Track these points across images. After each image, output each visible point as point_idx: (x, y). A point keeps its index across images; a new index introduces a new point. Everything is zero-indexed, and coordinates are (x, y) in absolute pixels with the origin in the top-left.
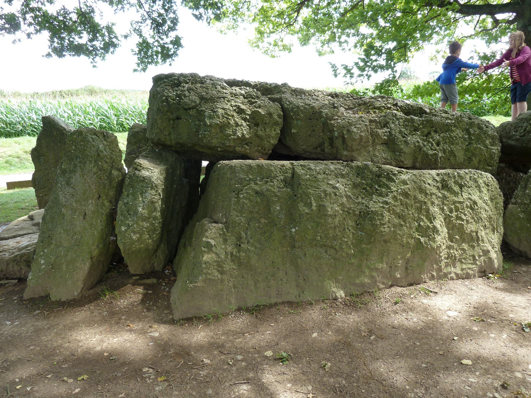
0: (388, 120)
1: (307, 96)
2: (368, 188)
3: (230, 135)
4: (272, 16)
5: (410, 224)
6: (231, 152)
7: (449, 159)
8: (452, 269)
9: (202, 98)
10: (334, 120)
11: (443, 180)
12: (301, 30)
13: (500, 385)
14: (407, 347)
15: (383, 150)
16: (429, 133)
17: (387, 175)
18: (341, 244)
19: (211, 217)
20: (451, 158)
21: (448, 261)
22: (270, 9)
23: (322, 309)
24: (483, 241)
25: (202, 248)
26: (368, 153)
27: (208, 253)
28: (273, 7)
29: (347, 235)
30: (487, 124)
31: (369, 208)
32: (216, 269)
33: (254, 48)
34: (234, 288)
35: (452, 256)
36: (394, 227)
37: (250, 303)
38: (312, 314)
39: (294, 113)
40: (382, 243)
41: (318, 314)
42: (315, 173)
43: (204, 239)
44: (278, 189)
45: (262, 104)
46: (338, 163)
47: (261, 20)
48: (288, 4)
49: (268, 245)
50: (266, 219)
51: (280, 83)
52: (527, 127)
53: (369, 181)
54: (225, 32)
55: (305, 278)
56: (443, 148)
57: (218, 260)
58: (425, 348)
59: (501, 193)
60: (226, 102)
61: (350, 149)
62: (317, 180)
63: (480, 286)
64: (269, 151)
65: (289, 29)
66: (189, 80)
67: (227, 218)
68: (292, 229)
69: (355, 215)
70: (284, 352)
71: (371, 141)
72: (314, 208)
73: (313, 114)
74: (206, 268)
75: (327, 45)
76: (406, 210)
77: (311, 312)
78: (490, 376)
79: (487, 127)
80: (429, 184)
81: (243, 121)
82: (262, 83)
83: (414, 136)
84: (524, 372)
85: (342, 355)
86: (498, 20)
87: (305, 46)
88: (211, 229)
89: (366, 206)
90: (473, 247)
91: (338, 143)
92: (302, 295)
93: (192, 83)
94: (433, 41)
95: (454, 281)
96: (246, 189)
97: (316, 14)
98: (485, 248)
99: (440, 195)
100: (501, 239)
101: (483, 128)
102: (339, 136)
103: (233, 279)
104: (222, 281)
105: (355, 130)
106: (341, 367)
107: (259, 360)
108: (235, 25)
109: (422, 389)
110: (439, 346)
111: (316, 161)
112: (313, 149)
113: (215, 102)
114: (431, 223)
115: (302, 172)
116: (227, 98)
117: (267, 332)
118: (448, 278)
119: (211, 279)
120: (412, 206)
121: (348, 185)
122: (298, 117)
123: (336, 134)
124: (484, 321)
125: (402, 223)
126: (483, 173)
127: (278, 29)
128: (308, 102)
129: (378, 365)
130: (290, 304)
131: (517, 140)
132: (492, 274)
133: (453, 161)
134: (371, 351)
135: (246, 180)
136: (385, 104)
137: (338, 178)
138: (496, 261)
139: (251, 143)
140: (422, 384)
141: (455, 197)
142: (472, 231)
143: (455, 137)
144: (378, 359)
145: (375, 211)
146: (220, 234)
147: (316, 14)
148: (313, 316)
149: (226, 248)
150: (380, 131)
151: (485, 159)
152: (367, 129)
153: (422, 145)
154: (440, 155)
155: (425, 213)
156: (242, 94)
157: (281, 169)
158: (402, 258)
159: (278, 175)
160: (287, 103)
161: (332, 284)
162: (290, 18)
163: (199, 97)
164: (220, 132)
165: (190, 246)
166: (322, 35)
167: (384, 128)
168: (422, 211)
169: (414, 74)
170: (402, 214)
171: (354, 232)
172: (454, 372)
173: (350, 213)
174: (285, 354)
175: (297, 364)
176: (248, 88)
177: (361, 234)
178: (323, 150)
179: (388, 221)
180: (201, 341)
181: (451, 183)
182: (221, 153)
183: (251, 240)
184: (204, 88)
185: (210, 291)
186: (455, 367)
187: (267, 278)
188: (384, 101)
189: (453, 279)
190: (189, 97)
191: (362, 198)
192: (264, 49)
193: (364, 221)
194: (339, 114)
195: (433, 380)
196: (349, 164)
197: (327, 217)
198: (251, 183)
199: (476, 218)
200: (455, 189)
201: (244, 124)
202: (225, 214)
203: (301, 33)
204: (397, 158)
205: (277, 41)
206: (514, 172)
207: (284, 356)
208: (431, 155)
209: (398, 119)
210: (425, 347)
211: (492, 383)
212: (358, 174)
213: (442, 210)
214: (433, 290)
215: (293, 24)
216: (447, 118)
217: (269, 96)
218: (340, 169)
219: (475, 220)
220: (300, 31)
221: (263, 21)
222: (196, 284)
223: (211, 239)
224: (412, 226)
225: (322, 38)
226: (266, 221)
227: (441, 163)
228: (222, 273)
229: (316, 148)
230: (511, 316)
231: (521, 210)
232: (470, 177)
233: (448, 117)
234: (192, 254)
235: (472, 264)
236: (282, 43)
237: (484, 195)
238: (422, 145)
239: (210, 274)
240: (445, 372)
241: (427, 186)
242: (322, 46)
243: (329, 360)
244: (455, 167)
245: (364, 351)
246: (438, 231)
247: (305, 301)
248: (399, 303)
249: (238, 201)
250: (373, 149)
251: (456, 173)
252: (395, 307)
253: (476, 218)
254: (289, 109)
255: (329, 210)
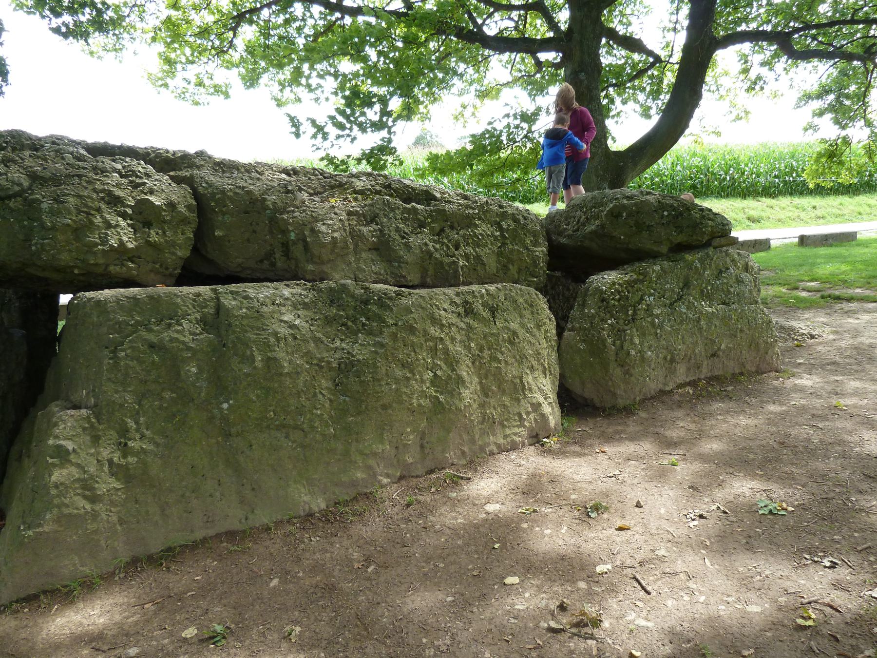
0: (377, 211)
1: (242, 173)
2: (350, 324)
3: (96, 245)
4: (189, 33)
5: (421, 376)
6: (102, 275)
7: (475, 270)
8: (491, 438)
9: (33, 177)
10: (288, 212)
11: (466, 302)
12: (243, 60)
13: (558, 607)
14: (425, 575)
15: (373, 260)
16: (442, 230)
17: (379, 300)
18: (311, 420)
19: (67, 399)
20: (479, 268)
21: (483, 426)
22: (184, 22)
23: (288, 535)
24: (530, 390)
25: (48, 458)
26: (348, 265)
27: (61, 466)
28: (190, 18)
29: (320, 404)
30: (525, 215)
31: (353, 356)
32: (79, 495)
33: (159, 89)
34: (121, 524)
35: (489, 418)
36: (396, 383)
37: (155, 546)
38: (271, 546)
39: (217, 202)
40: (380, 410)
41: (281, 544)
42: (256, 304)
43: (51, 442)
44: (191, 337)
45: (155, 187)
46: (298, 285)
47: (169, 40)
48: (217, 16)
49: (181, 437)
50: (173, 392)
51: (192, 151)
52: (581, 217)
53: (351, 312)
54: (98, 54)
55: (253, 486)
56: (465, 253)
57: (82, 477)
58: (452, 571)
59: (552, 316)
60: (85, 184)
61: (318, 261)
62: (261, 315)
63: (532, 459)
64: (175, 269)
65: (222, 58)
66: (6, 142)
67: (96, 397)
68: (222, 403)
69: (331, 369)
70: (219, 624)
71: (351, 246)
72: (259, 364)
73: (250, 203)
74: (58, 496)
75: (288, 89)
76: (413, 353)
77: (268, 543)
78: (544, 595)
79: (525, 219)
80: (445, 310)
81: (120, 219)
82: (159, 149)
83: (419, 235)
84: (590, 579)
85: (320, 608)
86: (541, 63)
87: (252, 89)
88: (64, 422)
89: (348, 353)
90: (518, 400)
91: (297, 251)
92: (251, 516)
93: (14, 149)
94: (454, 90)
95: (496, 456)
96: (130, 341)
97: (267, 36)
98: (534, 401)
99: (463, 325)
100: (557, 383)
101: (522, 221)
102: (298, 240)
103: (118, 509)
104: (95, 515)
105: (323, 228)
106: (317, 630)
107: (171, 648)
108: (117, 44)
109: (447, 637)
110: (472, 562)
111: (259, 284)
112: (257, 263)
113: (61, 185)
114: (453, 370)
115: (233, 303)
116: (86, 176)
117: (189, 594)
118: (486, 453)
119: (70, 515)
120: (421, 347)
121: (316, 321)
122: (224, 209)
123: (293, 236)
124: (537, 512)
125: (408, 375)
126: (524, 287)
127: (202, 58)
128: (240, 183)
129: (380, 612)
130: (231, 535)
131: (569, 236)
132: (548, 437)
133: (481, 273)
134: (368, 593)
135: (129, 325)
136: (372, 186)
137: (299, 310)
138: (551, 417)
139: (139, 257)
140: (446, 629)
141: (486, 326)
142: (514, 377)
143: (481, 234)
144: (378, 603)
145: (363, 359)
146: (84, 429)
147: (267, 36)
148: (272, 550)
149: (98, 453)
150: (365, 229)
151: (526, 267)
152: (343, 225)
153: (432, 249)
154: (461, 263)
155: (442, 357)
156: (116, 170)
157: (194, 300)
158: (413, 431)
159: (189, 312)
160: (203, 185)
161: (303, 490)
162: (222, 41)
163: (27, 175)
164: (75, 240)
165: (29, 457)
166: (281, 72)
167: (372, 225)
168: (438, 354)
169: (436, 139)
170: (407, 361)
171: (332, 397)
172: (493, 600)
173: (322, 367)
174: (219, 628)
175: (241, 642)
176: (128, 159)
177: (344, 401)
178: (273, 264)
179: (387, 374)
180: (56, 635)
181: (478, 306)
182: (82, 278)
183: (148, 433)
184: (38, 157)
185: (71, 537)
186: (495, 592)
187: (183, 496)
188: (371, 181)
189: (494, 454)
190: (6, 174)
191: (342, 340)
192: (179, 91)
193: (347, 377)
194: (297, 203)
195: (463, 620)
196: (316, 286)
197: (283, 378)
198: (140, 330)
199: (518, 357)
200: (484, 314)
201: (123, 223)
202: (94, 391)
203: (244, 67)
204: (396, 271)
205: (201, 76)
206: (573, 284)
207: (219, 631)
208: (447, 264)
209: (393, 210)
210: (453, 568)
211: (547, 605)
212: (332, 301)
213: (469, 348)
214: (465, 475)
215: (228, 50)
216: (467, 207)
217: (172, 173)
218: (301, 294)
219: (516, 360)
220: (240, 63)
221: (173, 42)
222: (41, 530)
223: (66, 439)
224: (425, 377)
225: (281, 77)
226: (174, 395)
227: (465, 275)
228: (93, 499)
229: (261, 261)
230: (573, 497)
231: (580, 339)
232: (505, 295)
233: (469, 205)
234: (31, 473)
235: (518, 427)
236: (212, 82)
237: (526, 320)
238: (432, 249)
239: (67, 506)
240: (481, 603)
241: (442, 313)
242: (281, 91)
243: (296, 622)
244: (485, 281)
245: (356, 596)
246: (463, 382)
247: (257, 526)
248: (412, 505)
249: (116, 364)
250: (355, 258)
251: (484, 291)
252: (407, 512)
253: (518, 357)
254: (206, 195)
255: (285, 365)
